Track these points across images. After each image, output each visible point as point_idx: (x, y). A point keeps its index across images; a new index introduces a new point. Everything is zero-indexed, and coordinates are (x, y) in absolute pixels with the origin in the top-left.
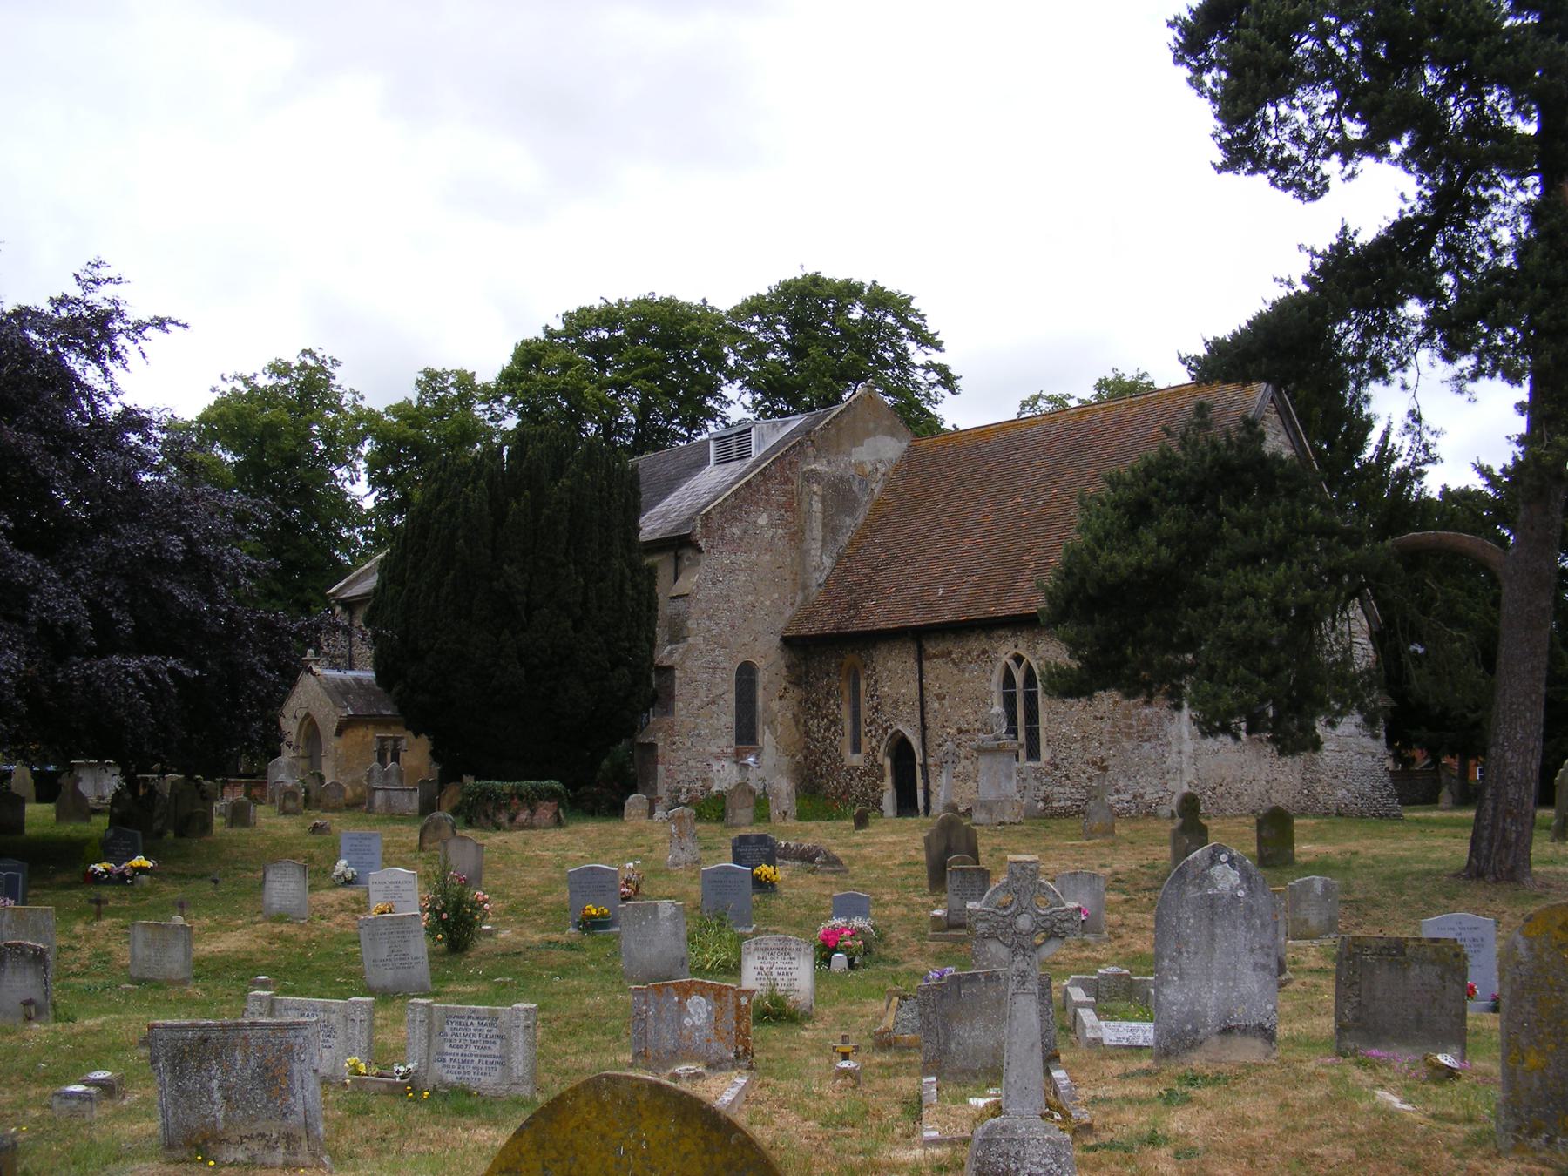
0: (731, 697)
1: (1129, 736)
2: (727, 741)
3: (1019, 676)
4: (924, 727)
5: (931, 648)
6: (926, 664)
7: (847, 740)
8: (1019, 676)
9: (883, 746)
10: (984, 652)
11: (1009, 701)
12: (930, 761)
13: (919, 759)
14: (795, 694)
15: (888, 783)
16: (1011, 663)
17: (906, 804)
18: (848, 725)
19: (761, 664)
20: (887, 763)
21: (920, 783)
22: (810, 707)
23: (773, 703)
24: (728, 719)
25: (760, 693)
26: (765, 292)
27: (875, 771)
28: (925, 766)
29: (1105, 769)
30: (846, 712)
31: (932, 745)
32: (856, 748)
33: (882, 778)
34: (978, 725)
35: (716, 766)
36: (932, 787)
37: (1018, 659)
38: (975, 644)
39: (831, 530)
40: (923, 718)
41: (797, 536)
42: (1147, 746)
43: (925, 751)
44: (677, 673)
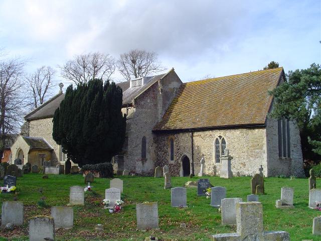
0: (141, 145)
1: (252, 157)
2: (140, 157)
3: (220, 141)
4: (193, 154)
5: (195, 134)
6: (194, 138)
7: (170, 157)
8: (220, 141)
9: (180, 159)
10: (211, 135)
11: (217, 148)
12: (194, 163)
13: (191, 161)
14: (155, 145)
15: (182, 168)
16: (218, 138)
17: (186, 172)
18: (170, 153)
19: (147, 137)
20: (181, 163)
21: (191, 168)
22: (159, 148)
23: (151, 148)
24: (140, 151)
25: (147, 145)
26: (307, 69)
27: (177, 165)
28: (193, 164)
29: (245, 165)
30: (169, 150)
31: (195, 158)
32: (172, 159)
33: (180, 167)
34: (209, 154)
35: (137, 163)
36: (195, 169)
37: (220, 137)
38: (208, 133)
39: (164, 104)
40: (193, 152)
41: (156, 105)
42: (257, 159)
43: (193, 160)
44: (129, 139)
